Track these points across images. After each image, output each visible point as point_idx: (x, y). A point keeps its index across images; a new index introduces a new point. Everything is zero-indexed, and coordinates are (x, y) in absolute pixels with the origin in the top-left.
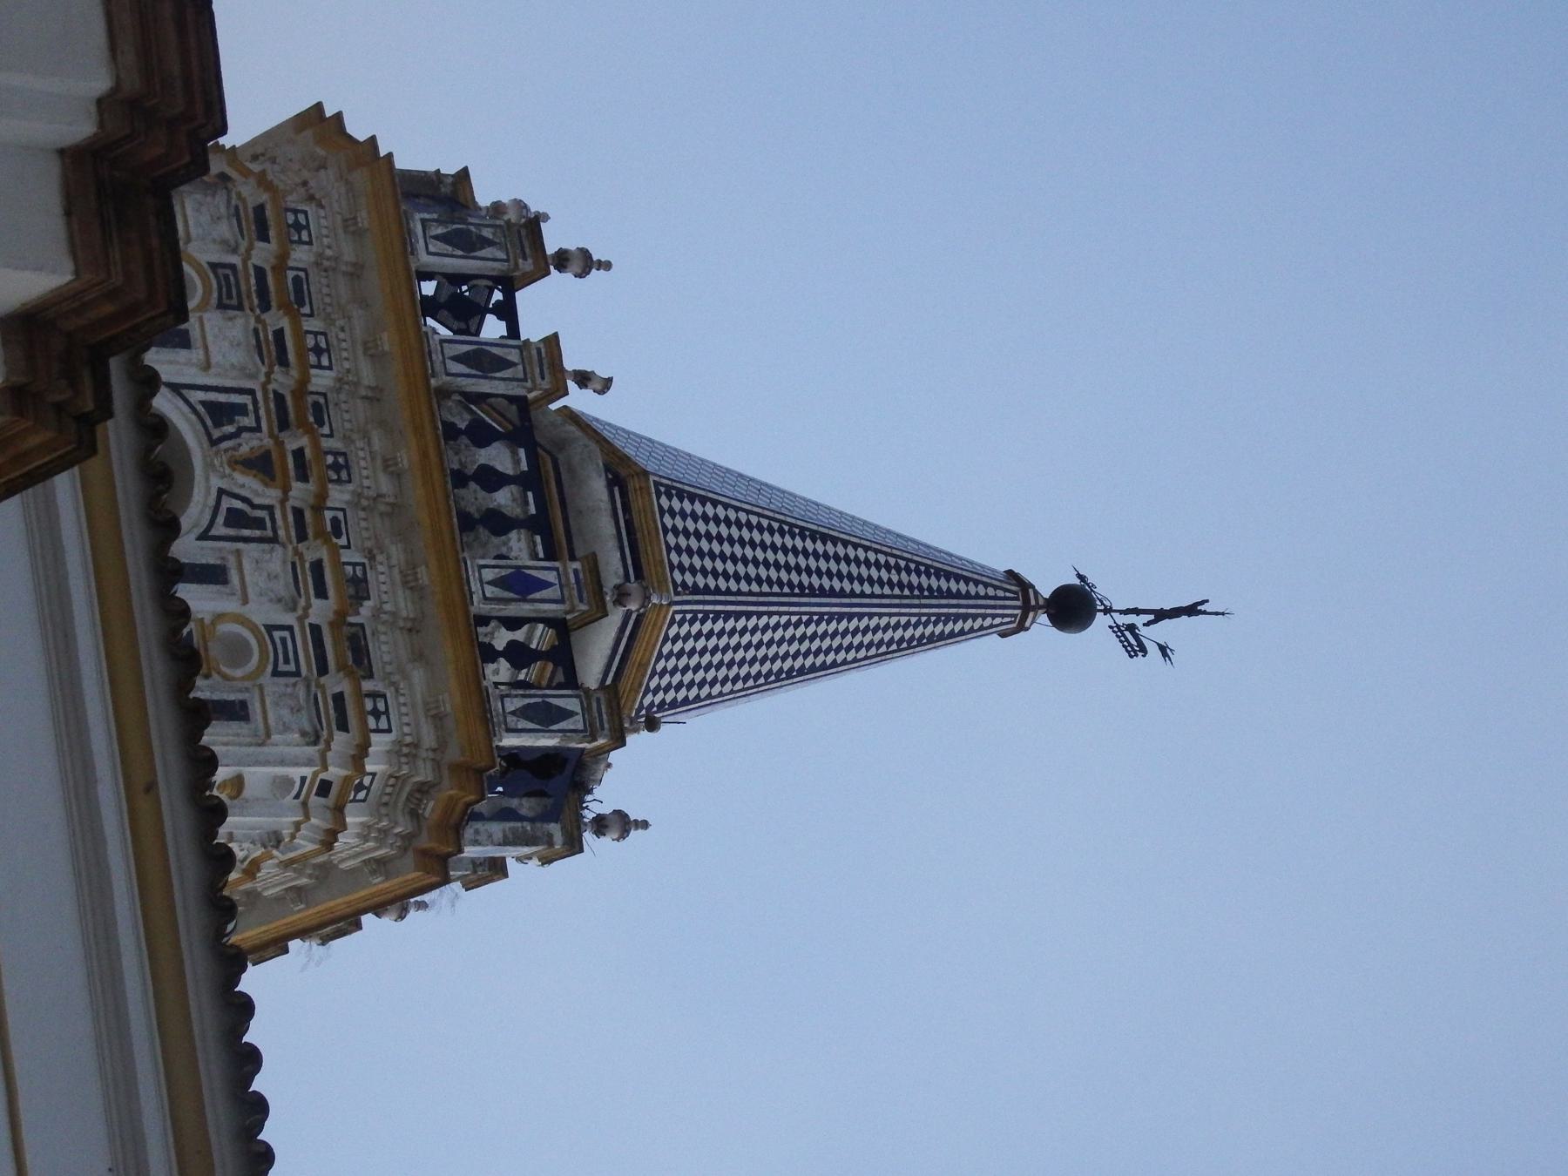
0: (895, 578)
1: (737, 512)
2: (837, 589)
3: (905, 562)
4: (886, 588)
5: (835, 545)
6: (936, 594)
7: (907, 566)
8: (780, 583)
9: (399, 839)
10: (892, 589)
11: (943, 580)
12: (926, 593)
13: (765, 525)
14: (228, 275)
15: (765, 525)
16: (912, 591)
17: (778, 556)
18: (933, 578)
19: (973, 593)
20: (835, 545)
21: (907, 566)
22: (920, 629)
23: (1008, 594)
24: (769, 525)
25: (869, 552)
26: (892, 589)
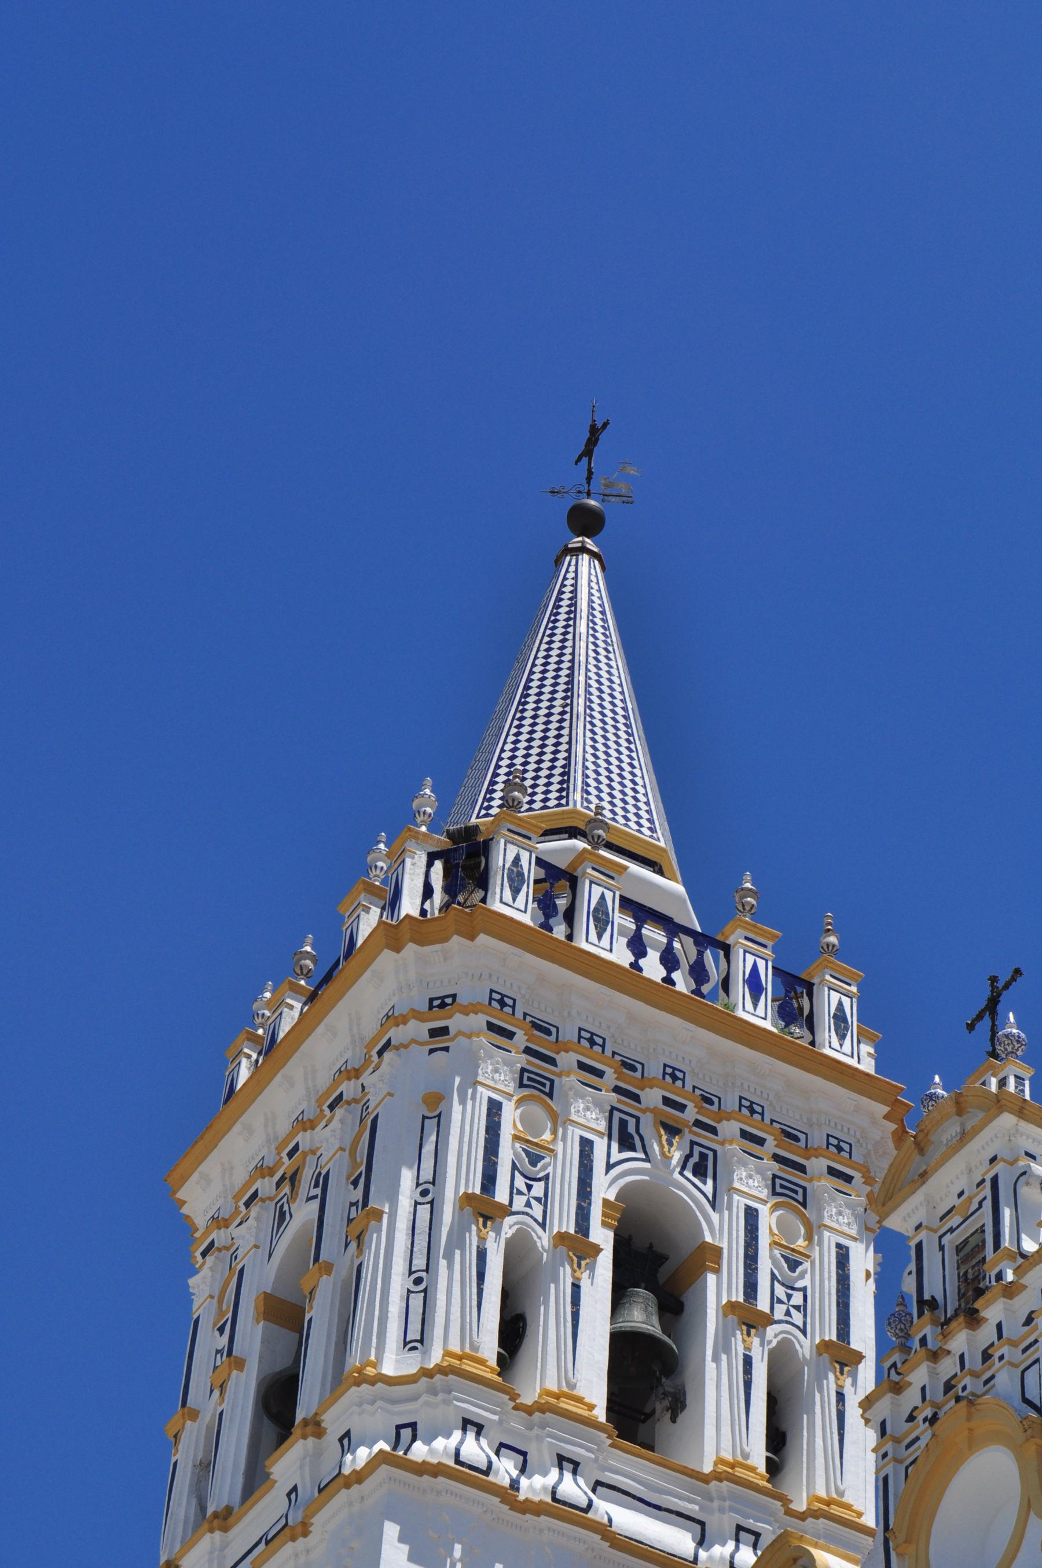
0: (538, 790)
1: (505, 751)
2: (568, 672)
3: (515, 721)
4: (564, 724)
5: (533, 680)
6: (570, 686)
7: (550, 629)
8: (566, 627)
9: (984, 1288)
10: (569, 633)
11: (528, 699)
12: (565, 786)
13: (548, 639)
14: (244, 1204)
15: (548, 639)
16: (567, 705)
17: (557, 643)
18: (493, 795)
19: (566, 755)
20: (533, 680)
21: (550, 629)
22: (597, 628)
23: (758, 1477)
24: (518, 719)
25: (505, 748)
26: (569, 633)
